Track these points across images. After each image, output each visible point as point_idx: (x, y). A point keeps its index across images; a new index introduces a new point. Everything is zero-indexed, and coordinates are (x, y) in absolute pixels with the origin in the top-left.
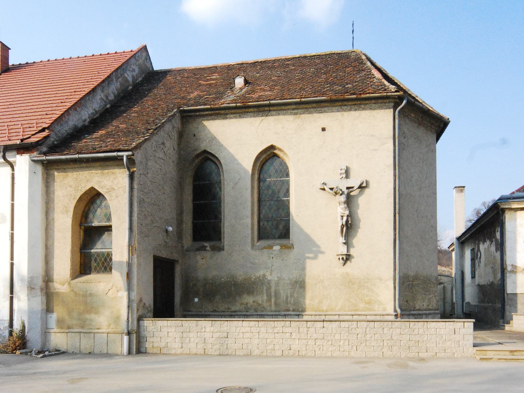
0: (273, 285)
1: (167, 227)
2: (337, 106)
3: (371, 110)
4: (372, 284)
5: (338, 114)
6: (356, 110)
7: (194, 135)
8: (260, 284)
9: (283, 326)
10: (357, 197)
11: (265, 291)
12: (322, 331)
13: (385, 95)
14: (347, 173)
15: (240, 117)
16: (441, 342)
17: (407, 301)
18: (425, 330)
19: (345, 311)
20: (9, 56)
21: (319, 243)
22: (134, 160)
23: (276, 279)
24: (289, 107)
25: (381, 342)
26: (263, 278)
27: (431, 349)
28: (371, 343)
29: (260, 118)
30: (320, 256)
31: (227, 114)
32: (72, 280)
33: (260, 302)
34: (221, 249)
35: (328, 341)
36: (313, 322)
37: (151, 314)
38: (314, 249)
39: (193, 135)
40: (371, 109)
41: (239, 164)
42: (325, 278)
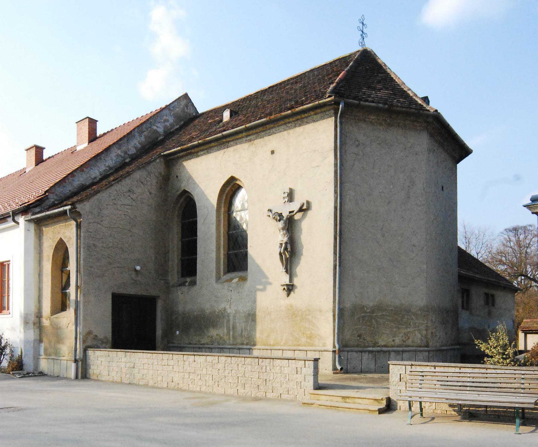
0: (231, 318)
1: (136, 266)
2: (281, 125)
3: (314, 122)
4: (313, 317)
5: (285, 133)
6: (300, 125)
7: (177, 177)
8: (222, 317)
9: (168, 358)
10: (301, 221)
11: (225, 325)
12: (194, 365)
13: (317, 104)
14: (291, 196)
15: (208, 153)
16: (285, 381)
17: (360, 336)
18: (271, 368)
19: (289, 346)
20: (97, 128)
21: (267, 274)
22: (79, 212)
23: (234, 312)
24: (240, 135)
25: (236, 378)
26: (224, 311)
27: (276, 389)
28: (229, 379)
29: (223, 150)
30: (269, 287)
31: (198, 152)
32: (52, 316)
33: (222, 335)
34: (193, 283)
35: (198, 375)
36: (187, 356)
37: (110, 345)
38: (263, 280)
39: (175, 176)
40: (314, 121)
41: (208, 199)
42: (272, 310)
